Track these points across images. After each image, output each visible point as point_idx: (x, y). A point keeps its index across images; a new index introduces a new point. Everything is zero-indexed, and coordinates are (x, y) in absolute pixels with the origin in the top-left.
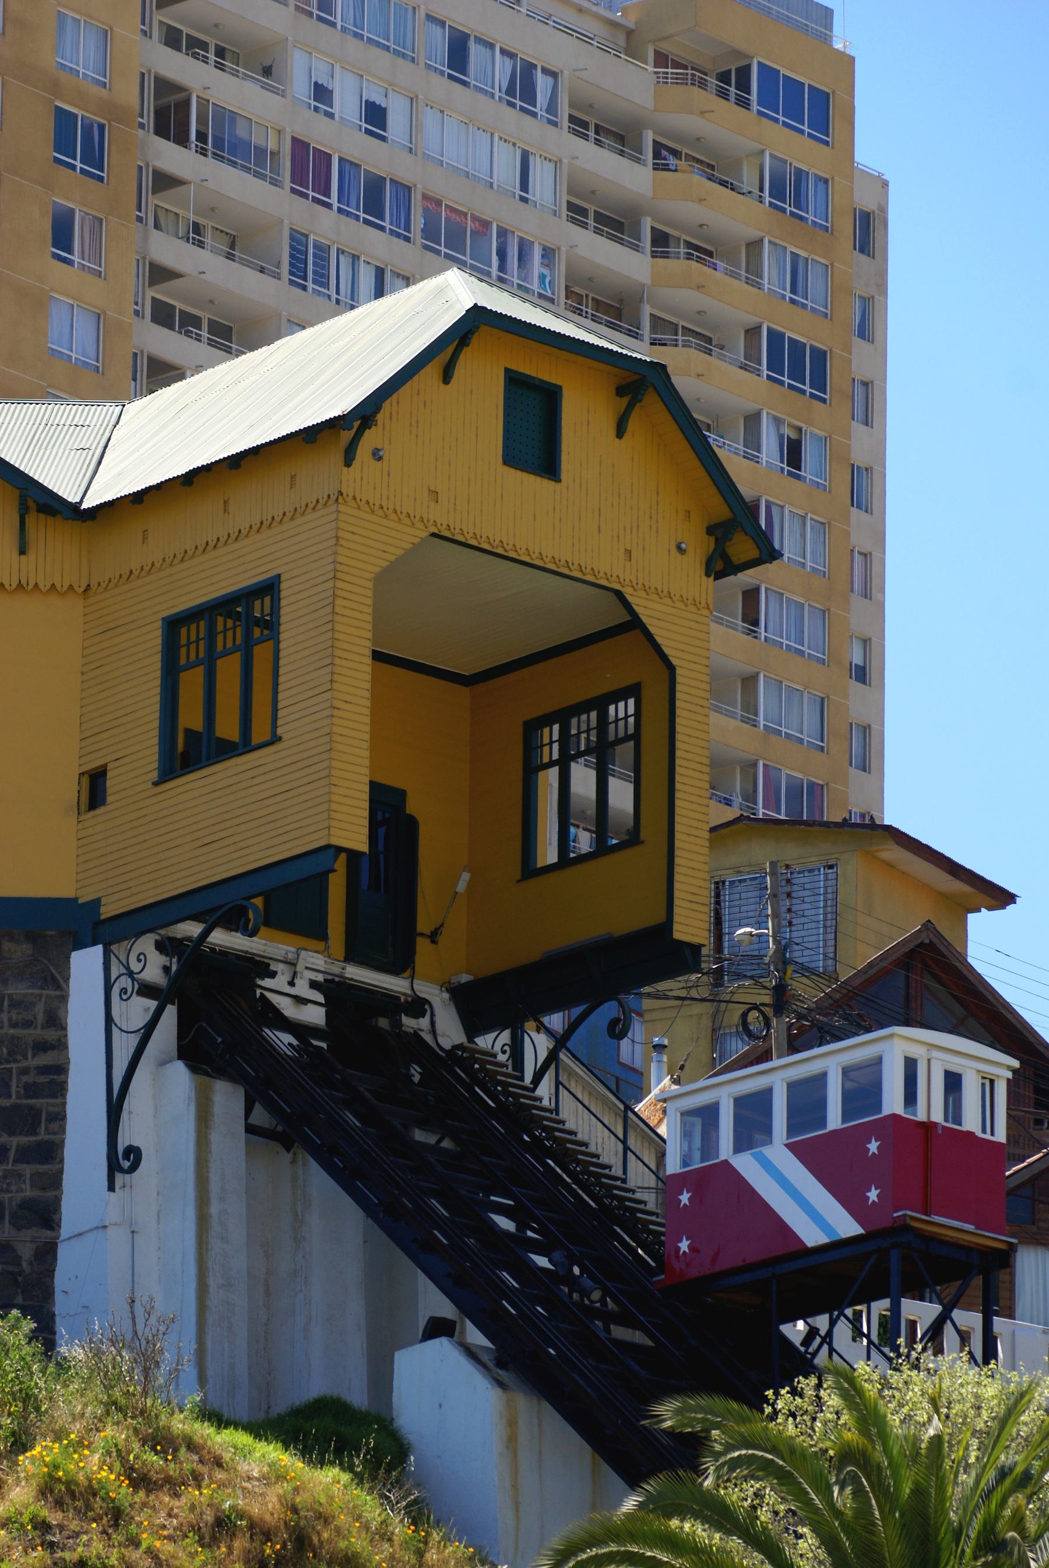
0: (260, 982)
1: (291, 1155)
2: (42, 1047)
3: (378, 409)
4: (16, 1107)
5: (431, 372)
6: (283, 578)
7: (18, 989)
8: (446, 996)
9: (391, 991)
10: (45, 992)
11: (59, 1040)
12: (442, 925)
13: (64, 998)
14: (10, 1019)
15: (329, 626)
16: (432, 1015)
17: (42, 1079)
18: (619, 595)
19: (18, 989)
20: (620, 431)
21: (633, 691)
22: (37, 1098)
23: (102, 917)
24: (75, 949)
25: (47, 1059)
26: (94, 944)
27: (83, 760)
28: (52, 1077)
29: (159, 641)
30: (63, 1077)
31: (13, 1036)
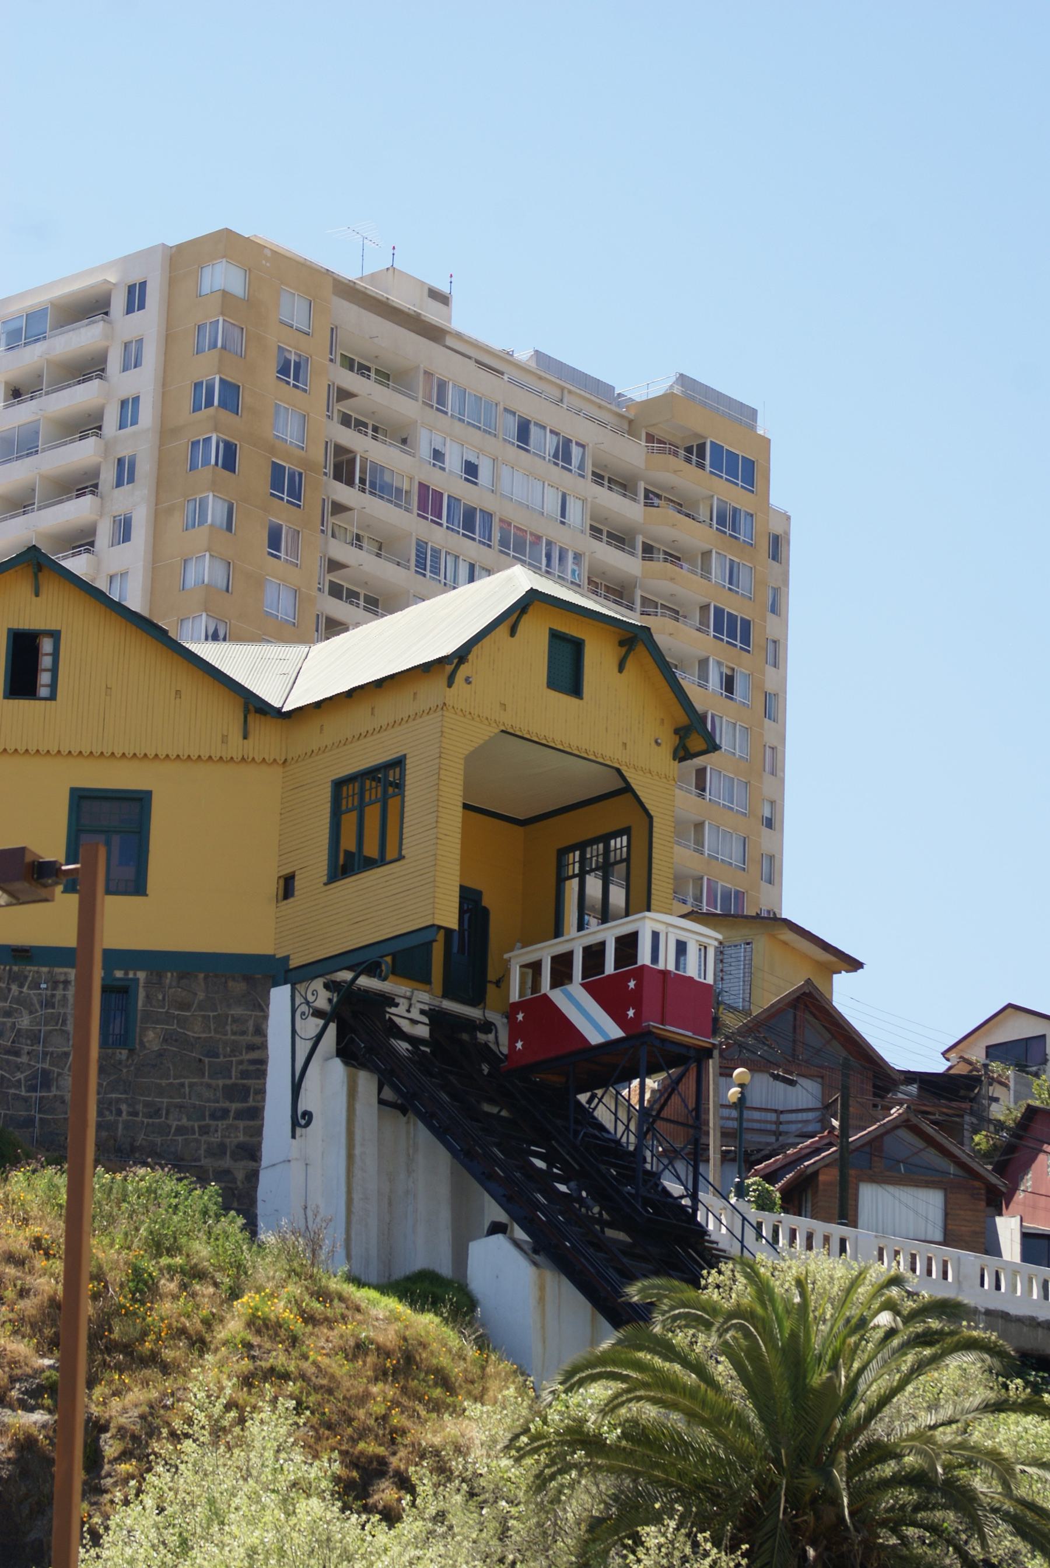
0: (389, 1010)
2: (252, 1048)
3: (469, 652)
4: (235, 1085)
5: (503, 630)
7: (237, 1011)
8: (505, 1020)
13: (266, 1017)
15: (436, 787)
19: (237, 1011)
20: (621, 668)
21: (626, 831)
25: (254, 1055)
26: (285, 983)
29: (329, 794)
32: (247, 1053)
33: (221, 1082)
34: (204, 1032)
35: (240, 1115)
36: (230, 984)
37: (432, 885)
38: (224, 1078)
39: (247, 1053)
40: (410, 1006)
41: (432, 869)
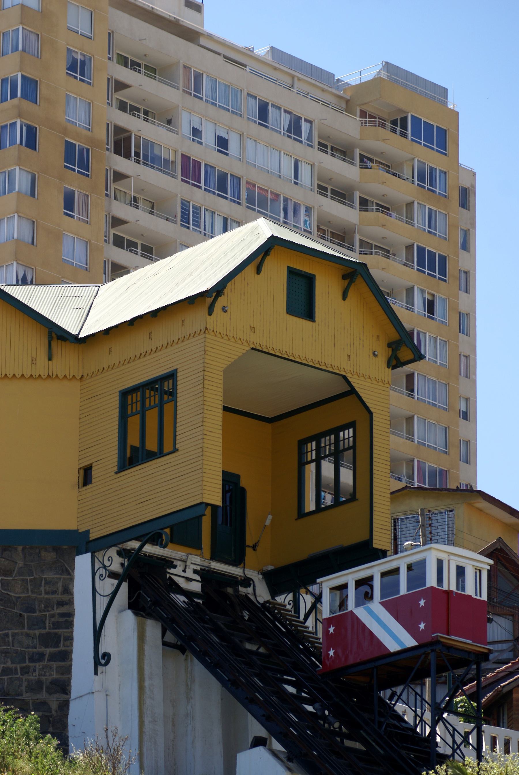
0: (168, 571)
1: (185, 656)
2: (61, 604)
4: (48, 634)
5: (251, 269)
6: (178, 371)
7: (49, 575)
8: (261, 576)
9: (234, 574)
10: (62, 576)
11: (70, 600)
12: (259, 541)
13: (72, 579)
14: (45, 590)
15: (201, 394)
16: (254, 586)
17: (61, 620)
18: (345, 377)
19: (49, 575)
20: (344, 297)
21: (352, 425)
22: (59, 629)
23: (91, 539)
24: (77, 555)
26: (87, 552)
27: (80, 461)
28: (66, 618)
29: (118, 402)
30: (72, 618)
31: (47, 598)
32: (57, 608)
33: (37, 632)
34: (23, 592)
35: (53, 657)
36: (43, 554)
37: (200, 471)
38: (40, 628)
39: (57, 608)
40: (186, 566)
41: (200, 458)
